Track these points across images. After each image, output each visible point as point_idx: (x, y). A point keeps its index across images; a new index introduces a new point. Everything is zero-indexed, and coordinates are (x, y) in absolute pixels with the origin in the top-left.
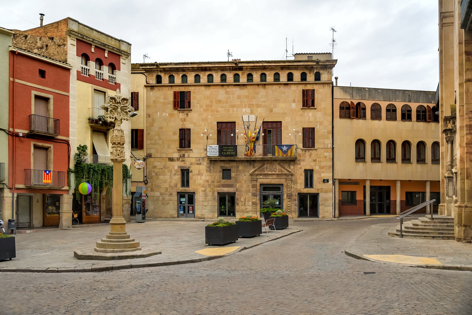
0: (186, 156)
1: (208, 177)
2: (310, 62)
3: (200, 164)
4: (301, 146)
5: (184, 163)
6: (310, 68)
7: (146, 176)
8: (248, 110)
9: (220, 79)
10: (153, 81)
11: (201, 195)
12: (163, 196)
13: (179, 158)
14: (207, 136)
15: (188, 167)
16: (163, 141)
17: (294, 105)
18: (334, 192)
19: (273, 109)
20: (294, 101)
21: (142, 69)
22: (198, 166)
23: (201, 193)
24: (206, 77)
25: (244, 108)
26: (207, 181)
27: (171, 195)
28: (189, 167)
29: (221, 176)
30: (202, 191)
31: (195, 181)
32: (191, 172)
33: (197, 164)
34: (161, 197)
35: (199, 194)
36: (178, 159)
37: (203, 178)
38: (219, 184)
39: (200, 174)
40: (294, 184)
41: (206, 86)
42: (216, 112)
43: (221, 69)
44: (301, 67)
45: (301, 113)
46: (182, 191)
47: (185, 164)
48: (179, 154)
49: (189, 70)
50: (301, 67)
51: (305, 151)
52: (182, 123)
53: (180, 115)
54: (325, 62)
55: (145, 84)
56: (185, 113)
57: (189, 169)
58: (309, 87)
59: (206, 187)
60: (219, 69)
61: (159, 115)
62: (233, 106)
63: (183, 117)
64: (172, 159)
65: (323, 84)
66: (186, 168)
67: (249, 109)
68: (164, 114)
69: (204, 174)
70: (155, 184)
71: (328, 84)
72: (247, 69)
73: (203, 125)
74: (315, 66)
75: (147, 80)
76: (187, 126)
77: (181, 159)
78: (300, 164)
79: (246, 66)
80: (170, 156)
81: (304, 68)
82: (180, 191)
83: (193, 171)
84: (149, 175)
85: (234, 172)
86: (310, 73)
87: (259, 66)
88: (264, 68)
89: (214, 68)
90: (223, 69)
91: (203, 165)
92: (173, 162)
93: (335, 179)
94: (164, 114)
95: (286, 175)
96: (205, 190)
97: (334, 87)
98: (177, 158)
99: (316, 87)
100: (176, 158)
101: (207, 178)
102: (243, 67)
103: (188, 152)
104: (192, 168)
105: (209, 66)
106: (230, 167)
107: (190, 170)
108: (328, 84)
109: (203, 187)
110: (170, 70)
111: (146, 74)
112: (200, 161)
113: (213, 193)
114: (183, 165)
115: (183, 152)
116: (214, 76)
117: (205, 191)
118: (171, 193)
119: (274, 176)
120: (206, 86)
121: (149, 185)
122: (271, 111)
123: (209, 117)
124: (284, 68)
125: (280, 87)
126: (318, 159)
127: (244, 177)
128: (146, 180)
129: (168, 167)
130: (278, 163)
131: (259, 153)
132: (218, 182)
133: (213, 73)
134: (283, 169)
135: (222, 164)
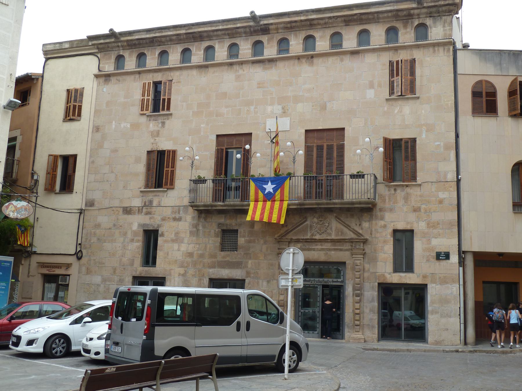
0: (155, 203)
3: (180, 219)
5: (150, 218)
14: (294, 157)
22: (175, 224)
28: (159, 226)
30: (180, 274)
32: (162, 235)
33: (175, 219)
53: (151, 125)
60: (225, 34)
63: (156, 128)
67: (280, 107)
83: (166, 234)
89: (215, 33)
91: (186, 221)
102: (271, 27)
103: (158, 196)
107: (160, 232)
122: (323, 107)
126: (423, 206)
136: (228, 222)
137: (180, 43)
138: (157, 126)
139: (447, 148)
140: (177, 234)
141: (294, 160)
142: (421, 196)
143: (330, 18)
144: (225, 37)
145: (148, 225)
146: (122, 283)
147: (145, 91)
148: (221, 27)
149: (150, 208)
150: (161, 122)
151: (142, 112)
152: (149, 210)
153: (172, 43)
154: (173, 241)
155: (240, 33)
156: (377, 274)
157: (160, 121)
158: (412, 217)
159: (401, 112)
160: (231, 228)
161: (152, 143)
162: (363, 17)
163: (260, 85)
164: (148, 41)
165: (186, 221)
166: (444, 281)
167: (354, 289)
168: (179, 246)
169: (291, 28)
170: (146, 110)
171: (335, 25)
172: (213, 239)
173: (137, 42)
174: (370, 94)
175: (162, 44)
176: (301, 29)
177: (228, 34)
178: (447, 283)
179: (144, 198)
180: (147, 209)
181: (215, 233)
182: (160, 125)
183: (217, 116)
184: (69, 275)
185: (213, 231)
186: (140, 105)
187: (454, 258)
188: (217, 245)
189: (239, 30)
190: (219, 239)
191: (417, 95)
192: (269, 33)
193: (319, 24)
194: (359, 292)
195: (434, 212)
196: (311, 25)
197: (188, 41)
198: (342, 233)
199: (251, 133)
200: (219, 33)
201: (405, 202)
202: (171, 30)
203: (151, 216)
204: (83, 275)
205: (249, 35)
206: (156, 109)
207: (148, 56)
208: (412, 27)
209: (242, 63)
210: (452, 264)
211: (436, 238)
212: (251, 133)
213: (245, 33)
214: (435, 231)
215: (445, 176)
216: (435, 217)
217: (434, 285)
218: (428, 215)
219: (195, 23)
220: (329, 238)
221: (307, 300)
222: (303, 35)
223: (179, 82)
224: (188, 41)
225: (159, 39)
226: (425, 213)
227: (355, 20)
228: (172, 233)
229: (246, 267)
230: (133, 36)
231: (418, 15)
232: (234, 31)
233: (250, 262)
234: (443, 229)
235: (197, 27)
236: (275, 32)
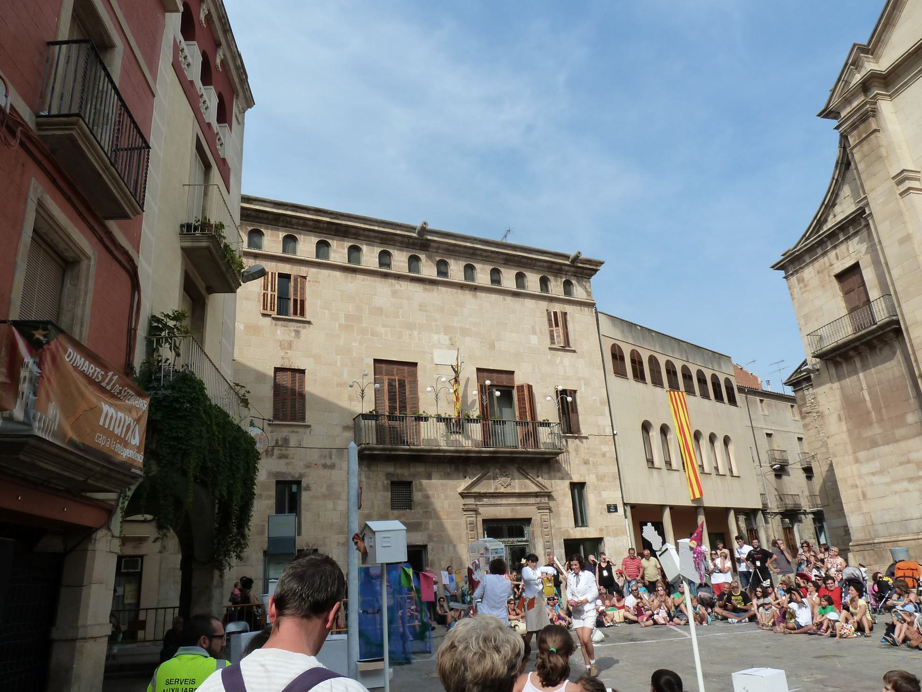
0: (292, 443)
3: (332, 467)
5: (287, 464)
14: (363, 391)
19: (496, 343)
22: (326, 472)
28: (301, 476)
30: (338, 544)
32: (308, 488)
33: (325, 466)
45: (549, 357)
53: (279, 331)
60: (376, 237)
62: (411, 326)
63: (287, 337)
67: (447, 337)
73: (339, 364)
83: (313, 487)
89: (367, 233)
91: (341, 469)
102: (432, 244)
103: (297, 432)
107: (304, 484)
122: (492, 346)
126: (591, 459)
127: (446, 503)
130: (516, 466)
136: (399, 471)
137: (315, 232)
138: (288, 334)
139: (602, 403)
140: (330, 487)
141: (362, 394)
142: (588, 449)
143: (493, 252)
144: (376, 241)
145: (284, 473)
146: (246, 562)
147: (267, 284)
148: (376, 228)
149: (286, 450)
150: (294, 330)
151: (265, 312)
152: (284, 452)
153: (304, 229)
154: (325, 497)
155: (395, 241)
156: (562, 529)
157: (292, 329)
158: (584, 469)
159: (562, 363)
160: (404, 480)
161: (283, 358)
162: (523, 260)
163: (422, 307)
164: (271, 217)
165: (341, 469)
166: (617, 533)
167: (545, 548)
168: (334, 503)
169: (453, 251)
170: (271, 310)
171: (494, 260)
172: (381, 493)
173: (253, 214)
174: (534, 339)
175: (289, 226)
176: (462, 255)
177: (381, 239)
178: (618, 535)
179: (275, 434)
180: (281, 450)
181: (383, 486)
182: (293, 334)
183: (372, 335)
184: (142, 557)
185: (380, 483)
186: (259, 301)
187: (621, 509)
188: (387, 501)
189: (396, 238)
190: (389, 494)
191: (307, 319)
192: (427, 251)
193: (481, 255)
194: (549, 550)
195: (600, 465)
196: (474, 254)
197: (327, 232)
198: (525, 486)
199: (417, 363)
200: (372, 234)
201: (577, 454)
202: (311, 212)
203: (288, 461)
204: (171, 554)
205: (404, 246)
206: (282, 310)
207: (267, 236)
208: (561, 281)
209: (476, 289)
210: (619, 516)
211: (605, 490)
212: (417, 363)
213: (402, 242)
214: (603, 484)
215: (604, 430)
216: (602, 470)
217: (609, 538)
218: (596, 468)
219: (346, 214)
220: (513, 491)
221: (524, 561)
222: (348, 244)
223: (317, 282)
224: (327, 232)
225: (289, 219)
226: (593, 466)
227: (514, 261)
228: (323, 486)
229: (427, 529)
230: (251, 204)
231: (567, 271)
232: (390, 237)
233: (431, 522)
234: (609, 482)
235: (347, 218)
236: (435, 251)
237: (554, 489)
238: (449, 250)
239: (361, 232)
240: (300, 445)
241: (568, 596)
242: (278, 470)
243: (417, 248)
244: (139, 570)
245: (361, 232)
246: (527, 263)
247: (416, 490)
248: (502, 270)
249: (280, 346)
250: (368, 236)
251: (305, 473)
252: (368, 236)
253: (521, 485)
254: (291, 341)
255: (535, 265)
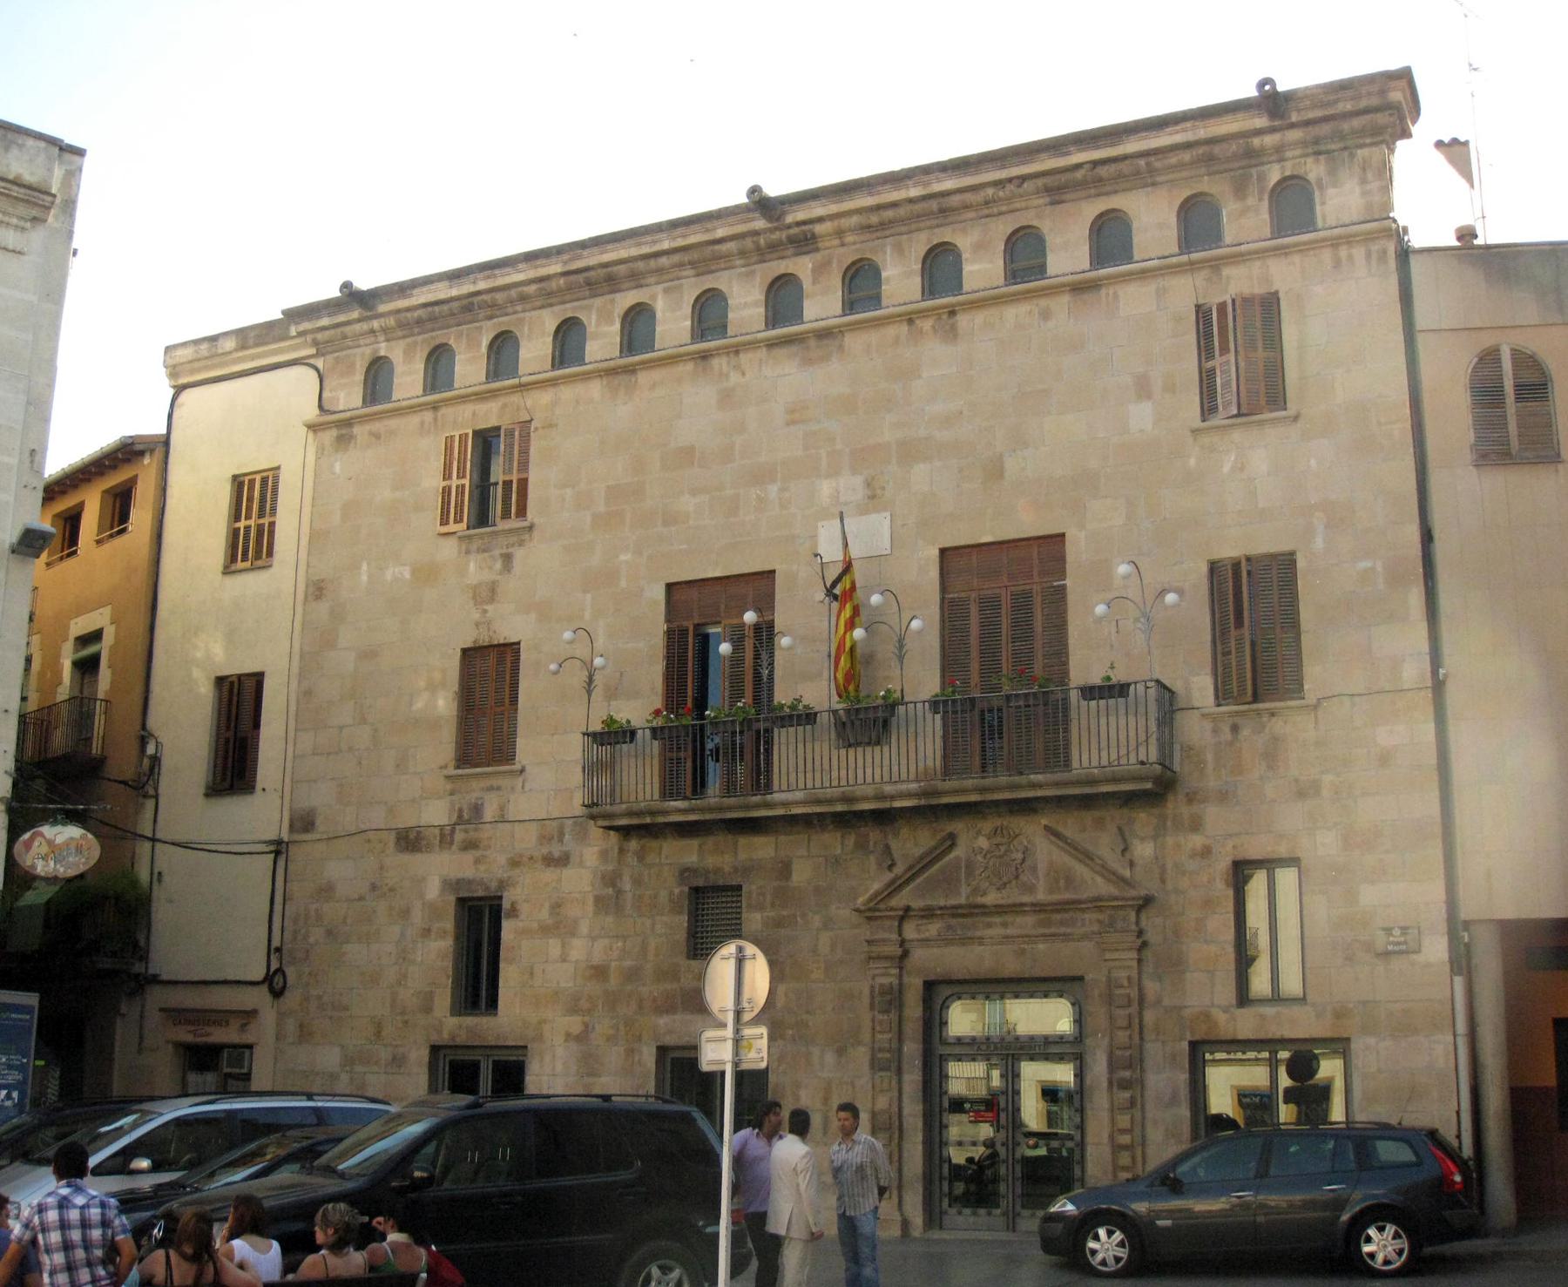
0: (489, 813)
1: (606, 941)
2: (1230, 117)
3: (563, 861)
4: (1200, 688)
5: (477, 861)
6: (1235, 157)
7: (278, 950)
8: (850, 486)
9: (688, 323)
10: (348, 397)
11: (559, 1067)
12: (359, 1068)
13: (453, 831)
15: (494, 885)
16: (376, 730)
17: (1141, 417)
18: (1461, 1027)
19: (1011, 465)
20: (1143, 389)
21: (300, 334)
22: (549, 875)
23: (560, 1051)
24: (617, 326)
25: (828, 476)
26: (600, 972)
27: (398, 1061)
28: (503, 884)
29: (681, 936)
30: (568, 1036)
31: (532, 974)
32: (514, 912)
33: (550, 861)
34: (344, 1077)
35: (547, 1059)
36: (446, 838)
37: (578, 949)
38: (668, 986)
39: (560, 927)
40: (1160, 979)
41: (612, 372)
42: (666, 523)
43: (692, 264)
44: (1173, 160)
46: (459, 1041)
47: (482, 868)
48: (452, 804)
49: (523, 298)
50: (1173, 160)
51: (1235, 729)
52: (476, 616)
53: (472, 565)
54: (1332, 97)
55: (312, 413)
56: (497, 552)
57: (500, 898)
58: (1240, 282)
59: (589, 1011)
60: (681, 265)
61: (364, 578)
62: (761, 476)
63: (487, 576)
64: (412, 836)
65: (1335, 243)
66: (487, 888)
67: (858, 481)
68: (389, 575)
69: (584, 928)
70: (319, 997)
71: (1369, 238)
72: (840, 233)
74: (1269, 140)
75: (325, 395)
76: (510, 626)
77: (459, 836)
78: (1196, 825)
79: (832, 217)
80: (407, 820)
81: (1194, 163)
82: (444, 1038)
83: (524, 909)
84: (295, 939)
85: (760, 907)
86: (1240, 190)
87: (911, 201)
88: (941, 209)
89: (653, 263)
90: (1060, 189)
91: (581, 864)
92: (419, 856)
93: (1467, 925)
94: (389, 575)
95: (1097, 903)
96: (587, 1029)
97: (1414, 260)
98: (441, 827)
99: (1282, 275)
100: (437, 831)
101: (599, 952)
102: (819, 229)
103: (499, 788)
104: (519, 890)
105: (623, 253)
106: (736, 870)
107: (506, 905)
108: (1369, 238)
109: (573, 1009)
110: (468, 308)
111: (320, 363)
112: (561, 840)
113: (630, 1052)
114: (469, 873)
115: (474, 791)
116: (659, 315)
117: (582, 1038)
118: (401, 1050)
119: (1019, 919)
120: (612, 372)
121: (292, 999)
122: (995, 471)
123: (623, 557)
124: (1060, 189)
125: (1046, 315)
126: (1328, 779)
127: (825, 939)
128: (280, 970)
129: (391, 890)
131: (921, 765)
132: (662, 975)
133: (654, 297)
134: (1081, 870)
135: (687, 853)
145: (470, 882)
149: (476, 830)
150: (501, 555)
151: (445, 529)
154: (546, 930)
165: (581, 864)
168: (563, 946)
184: (250, 1047)
185: (664, 894)
203: (478, 853)
206: (482, 518)
217: (1371, 1041)
224: (575, 296)
228: (542, 905)
237: (1169, 886)
238: (869, 227)
239: (641, 265)
240: (503, 816)
241: (715, 737)
242: (460, 875)
243: (789, 252)
244: (245, 1070)
245: (641, 265)
246: (1120, 176)
247: (749, 906)
248: (1045, 226)
249: (474, 598)
250: (660, 271)
251: (509, 878)
252: (660, 271)
253: (1057, 881)
254: (494, 582)
255: (1152, 171)
